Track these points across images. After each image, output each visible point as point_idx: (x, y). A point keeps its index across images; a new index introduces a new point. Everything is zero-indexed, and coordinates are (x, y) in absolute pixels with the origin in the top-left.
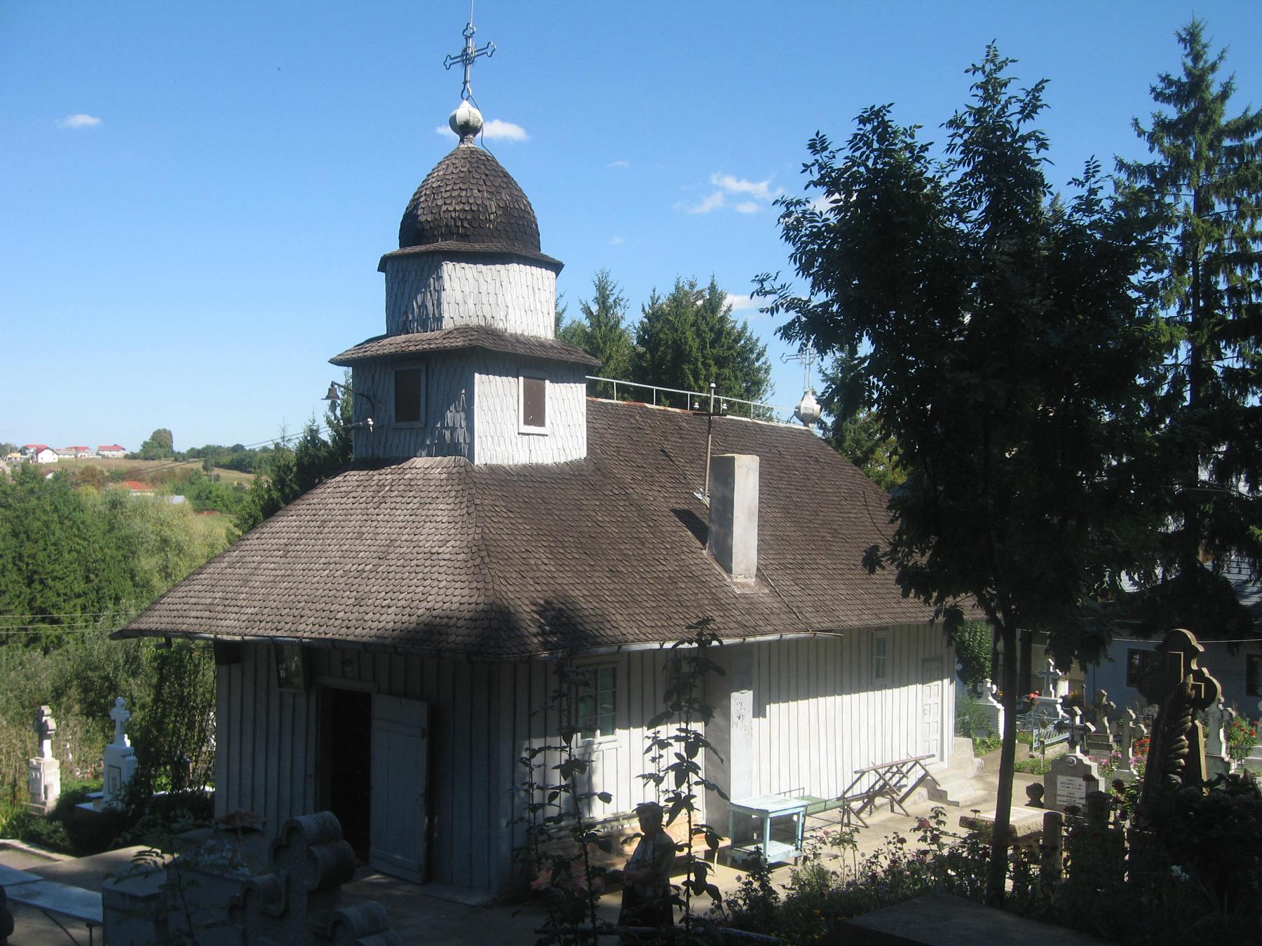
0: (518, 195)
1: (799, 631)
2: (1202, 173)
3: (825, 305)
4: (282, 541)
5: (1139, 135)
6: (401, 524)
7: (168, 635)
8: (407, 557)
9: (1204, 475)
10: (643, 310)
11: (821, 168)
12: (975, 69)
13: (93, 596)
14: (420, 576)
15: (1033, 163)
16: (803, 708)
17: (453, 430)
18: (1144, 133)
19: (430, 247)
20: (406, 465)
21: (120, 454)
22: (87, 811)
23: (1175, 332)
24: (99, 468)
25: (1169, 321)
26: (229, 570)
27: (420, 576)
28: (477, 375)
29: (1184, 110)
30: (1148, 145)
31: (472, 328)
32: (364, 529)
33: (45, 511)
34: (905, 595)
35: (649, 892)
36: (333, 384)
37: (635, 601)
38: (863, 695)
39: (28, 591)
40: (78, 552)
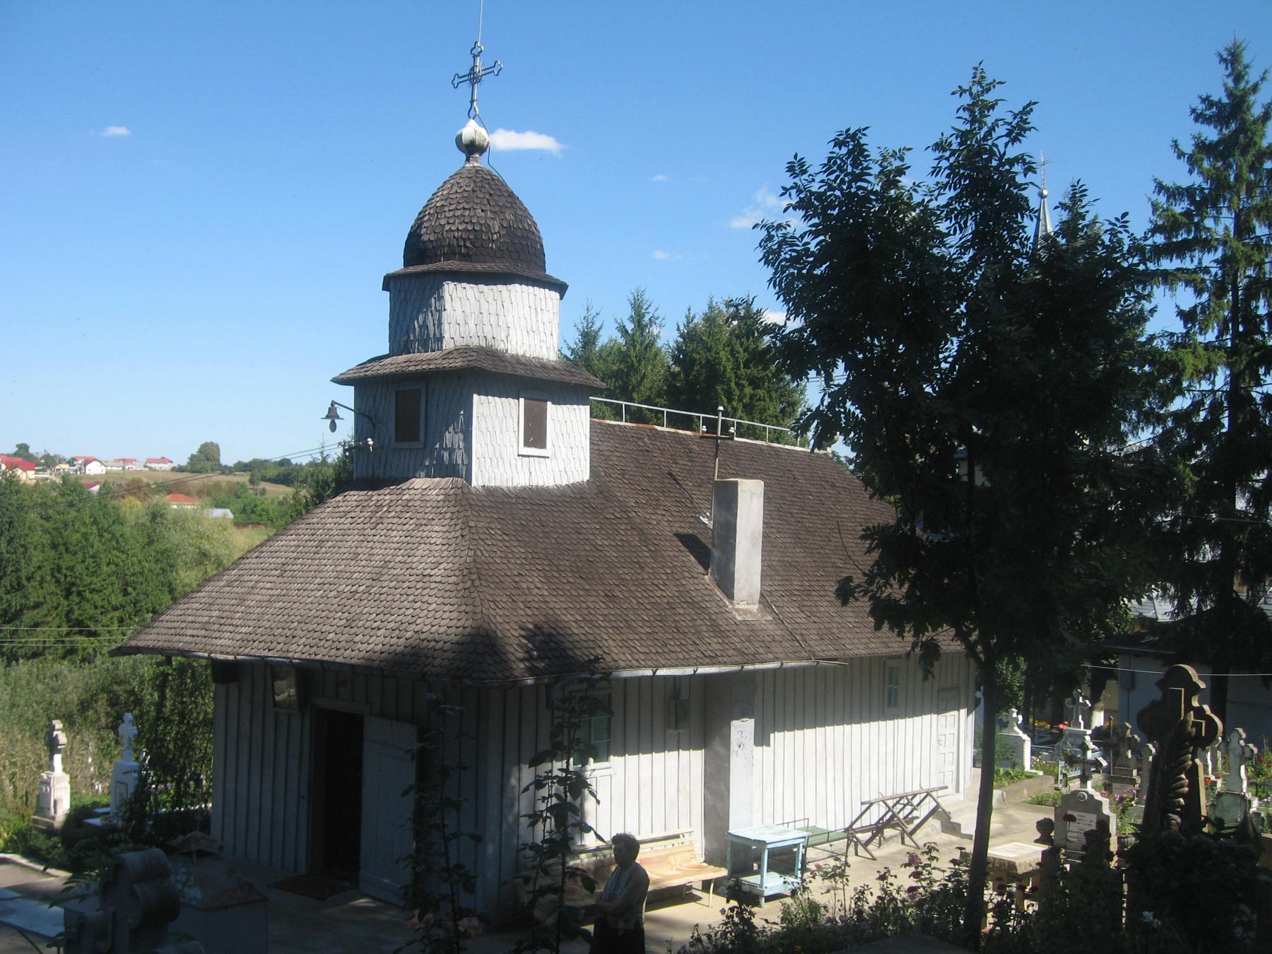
0: (523, 214)
1: (801, 659)
2: (1243, 196)
3: (801, 330)
4: (280, 561)
5: (1179, 157)
6: (396, 546)
7: (167, 655)
8: (400, 578)
9: (1240, 504)
10: (678, 329)
11: (799, 192)
12: (962, 91)
13: (130, 609)
14: (411, 598)
15: (1020, 187)
16: (809, 736)
17: (451, 451)
18: (1184, 155)
19: (432, 267)
20: (404, 486)
21: (168, 466)
22: (94, 827)
23: (1214, 358)
24: (145, 480)
25: (1207, 346)
26: (227, 589)
27: (411, 598)
28: (475, 396)
29: (1224, 131)
30: (1187, 167)
31: (472, 349)
32: (359, 550)
33: (84, 524)
34: (878, 627)
35: (621, 925)
36: (333, 403)
37: (630, 627)
38: (874, 724)
39: (66, 603)
40: (117, 565)
